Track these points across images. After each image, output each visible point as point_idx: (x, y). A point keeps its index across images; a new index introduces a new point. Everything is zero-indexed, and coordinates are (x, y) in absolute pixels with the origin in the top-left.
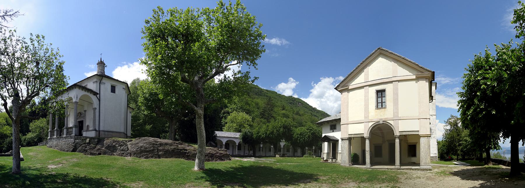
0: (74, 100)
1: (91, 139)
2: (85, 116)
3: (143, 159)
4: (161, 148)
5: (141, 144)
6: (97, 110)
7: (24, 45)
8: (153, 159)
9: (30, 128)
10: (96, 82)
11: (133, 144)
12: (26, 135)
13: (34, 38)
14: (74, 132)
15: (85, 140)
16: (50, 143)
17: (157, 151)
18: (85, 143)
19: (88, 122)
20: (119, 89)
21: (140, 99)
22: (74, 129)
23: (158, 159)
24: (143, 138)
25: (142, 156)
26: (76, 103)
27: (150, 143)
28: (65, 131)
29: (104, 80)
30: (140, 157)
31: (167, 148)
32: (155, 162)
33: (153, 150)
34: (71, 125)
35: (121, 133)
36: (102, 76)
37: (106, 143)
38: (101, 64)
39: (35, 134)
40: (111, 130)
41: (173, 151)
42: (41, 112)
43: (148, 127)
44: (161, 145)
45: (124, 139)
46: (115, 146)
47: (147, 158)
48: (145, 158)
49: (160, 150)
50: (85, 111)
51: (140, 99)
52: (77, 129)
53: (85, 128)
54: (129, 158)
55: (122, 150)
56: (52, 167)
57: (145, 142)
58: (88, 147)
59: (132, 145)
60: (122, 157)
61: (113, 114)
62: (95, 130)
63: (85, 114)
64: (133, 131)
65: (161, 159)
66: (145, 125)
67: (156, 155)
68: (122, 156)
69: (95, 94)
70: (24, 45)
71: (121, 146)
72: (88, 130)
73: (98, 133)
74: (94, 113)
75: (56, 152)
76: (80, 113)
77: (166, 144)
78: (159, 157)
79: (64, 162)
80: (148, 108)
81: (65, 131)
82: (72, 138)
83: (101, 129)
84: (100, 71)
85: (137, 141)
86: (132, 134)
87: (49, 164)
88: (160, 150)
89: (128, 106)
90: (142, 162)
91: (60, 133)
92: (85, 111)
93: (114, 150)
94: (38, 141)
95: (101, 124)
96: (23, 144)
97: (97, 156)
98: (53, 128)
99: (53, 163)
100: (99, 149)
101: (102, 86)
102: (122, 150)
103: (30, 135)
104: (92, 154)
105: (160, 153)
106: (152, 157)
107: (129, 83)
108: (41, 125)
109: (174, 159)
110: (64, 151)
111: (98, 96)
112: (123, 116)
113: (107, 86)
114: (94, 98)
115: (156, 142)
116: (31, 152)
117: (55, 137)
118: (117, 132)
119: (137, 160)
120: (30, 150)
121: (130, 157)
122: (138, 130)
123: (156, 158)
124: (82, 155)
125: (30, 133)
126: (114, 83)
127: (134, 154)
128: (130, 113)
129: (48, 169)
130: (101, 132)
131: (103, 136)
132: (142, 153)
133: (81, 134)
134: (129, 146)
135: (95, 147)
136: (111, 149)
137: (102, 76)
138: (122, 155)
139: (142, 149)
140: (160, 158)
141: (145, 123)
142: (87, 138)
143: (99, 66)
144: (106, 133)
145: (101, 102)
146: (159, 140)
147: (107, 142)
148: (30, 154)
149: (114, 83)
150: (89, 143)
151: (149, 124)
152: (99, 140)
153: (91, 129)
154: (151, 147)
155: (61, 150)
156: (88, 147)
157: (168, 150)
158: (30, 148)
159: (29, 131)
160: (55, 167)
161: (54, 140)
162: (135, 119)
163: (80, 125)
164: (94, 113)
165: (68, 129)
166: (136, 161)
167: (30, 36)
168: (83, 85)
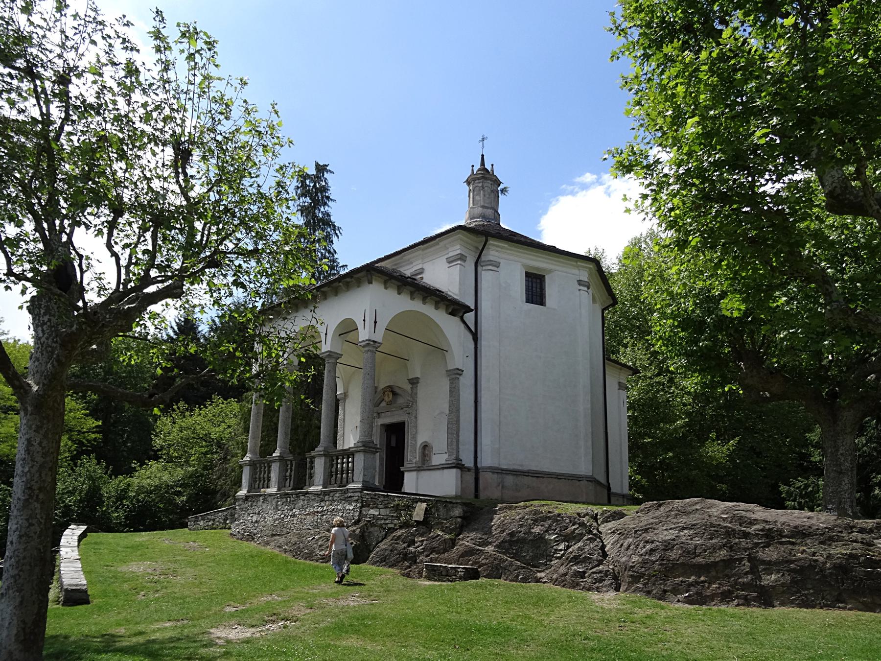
0: (364, 335)
1: (436, 503)
2: (411, 405)
3: (677, 607)
4: (770, 554)
5: (665, 534)
6: (466, 382)
7: (121, 56)
8: (729, 609)
9: (158, 442)
10: (462, 258)
11: (630, 531)
12: (130, 472)
13: (172, 33)
14: (359, 475)
15: (409, 508)
16: (247, 519)
17: (753, 570)
18: (406, 525)
19: (428, 429)
20: (561, 286)
21: (661, 326)
22: (359, 459)
23: (757, 611)
24: (677, 503)
25: (676, 591)
26: (372, 345)
27: (712, 529)
28: (319, 466)
29: (495, 251)
30: (662, 596)
31: (803, 552)
32: (736, 625)
33: (728, 563)
34: (349, 439)
35: (577, 478)
36: (485, 234)
37: (503, 527)
38: (485, 182)
39: (180, 473)
40: (533, 466)
41: (843, 568)
42: (196, 372)
43: (717, 450)
44: (771, 536)
45: (582, 508)
46: (540, 538)
47: (699, 599)
48: (689, 601)
49: (770, 566)
50: (414, 382)
51: (661, 326)
52: (378, 460)
53: (412, 457)
54: (608, 600)
55: (576, 560)
56: (232, 635)
57: (683, 520)
58: (420, 544)
59: (623, 534)
60: (576, 593)
61: (535, 398)
62: (459, 465)
63: (414, 395)
64: (641, 470)
65: (778, 611)
66: (703, 438)
67: (744, 587)
68: (575, 585)
69: (456, 308)
70: (121, 56)
71: (570, 538)
72: (425, 465)
73: (470, 477)
74: (454, 392)
75: (272, 559)
76: (393, 391)
77: (800, 534)
78: (766, 598)
79: (298, 610)
80: (703, 361)
81: (319, 466)
82: (349, 500)
83: (486, 460)
84: (479, 210)
85: (646, 519)
86: (633, 485)
87: (220, 619)
88: (770, 566)
89: (609, 355)
90: (669, 620)
91: (298, 477)
92: (414, 382)
93: (536, 557)
94: (201, 500)
95: (486, 440)
96: (106, 515)
97: (459, 585)
98: (267, 448)
99: (240, 618)
100: (470, 552)
101: (486, 277)
102: (576, 560)
103: (151, 475)
104: (435, 574)
105: (769, 579)
106: (726, 597)
107: (611, 262)
108: (215, 432)
109: (852, 615)
110: (310, 556)
111: (469, 317)
112: (583, 405)
113: (508, 272)
114: (451, 328)
115: (741, 521)
116: (143, 557)
117: (273, 490)
118: (558, 476)
119: (646, 607)
120: (135, 547)
121: (612, 594)
122: (665, 466)
123: (747, 602)
124: (390, 575)
125: (154, 466)
126: (538, 262)
127: (635, 579)
128: (622, 387)
129: (211, 644)
130: (484, 477)
131: (496, 494)
132: (667, 575)
133: (394, 481)
134: (609, 541)
135: (453, 543)
136: (526, 555)
137: (485, 234)
138: (574, 581)
139: (673, 555)
140: (749, 605)
141: (699, 430)
142: (416, 498)
143: (473, 192)
144: (510, 480)
145: (484, 343)
146: (758, 512)
147: (506, 519)
148: (137, 567)
149: (538, 262)
150: (426, 524)
151: (723, 437)
152: (473, 511)
153: (438, 459)
154: (714, 549)
155: (297, 552)
156: (420, 544)
157: (812, 565)
158: (143, 537)
159: (148, 454)
160: (248, 633)
161: (268, 507)
162: (647, 414)
163: (392, 446)
164: (454, 392)
165: (334, 456)
166: (640, 613)
167: (150, 24)
168: (408, 271)
